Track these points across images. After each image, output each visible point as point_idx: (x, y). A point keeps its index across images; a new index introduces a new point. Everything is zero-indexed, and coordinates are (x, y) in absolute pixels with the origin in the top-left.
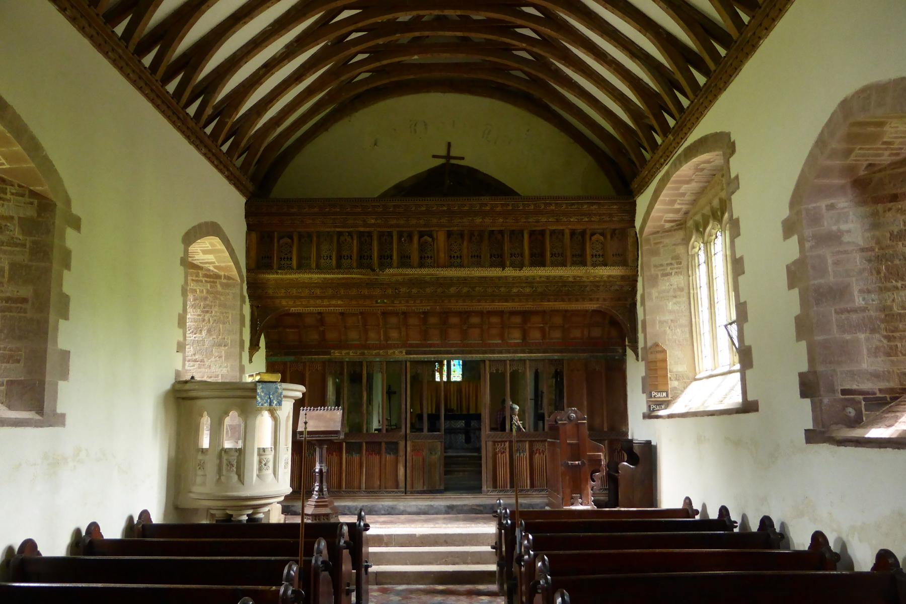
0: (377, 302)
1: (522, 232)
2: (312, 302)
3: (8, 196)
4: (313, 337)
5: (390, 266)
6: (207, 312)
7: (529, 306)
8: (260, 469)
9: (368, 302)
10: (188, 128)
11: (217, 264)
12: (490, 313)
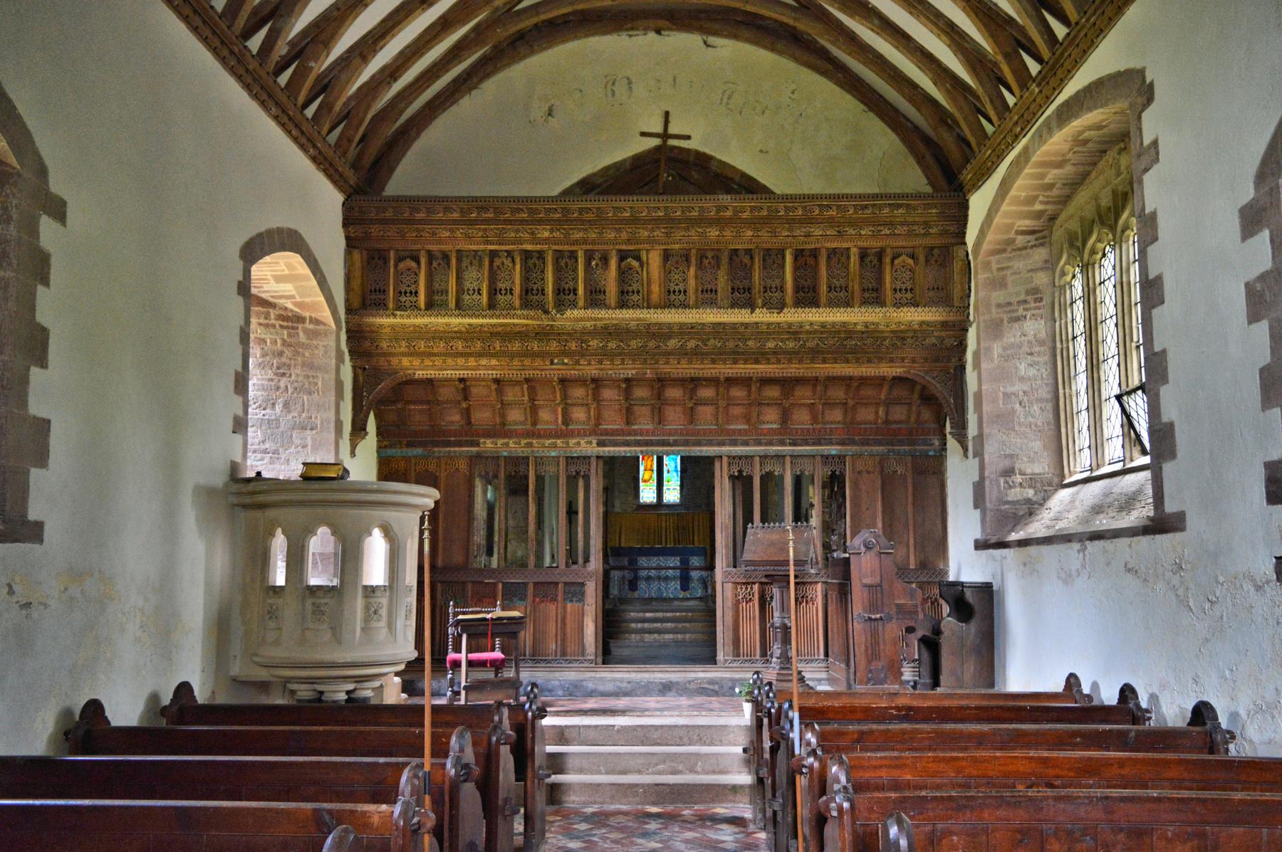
0: (552, 363)
1: (782, 253)
4: (454, 418)
5: (574, 305)
6: (284, 374)
7: (793, 370)
8: (367, 619)
9: (538, 362)
10: (247, 70)
11: (298, 299)
12: (731, 381)
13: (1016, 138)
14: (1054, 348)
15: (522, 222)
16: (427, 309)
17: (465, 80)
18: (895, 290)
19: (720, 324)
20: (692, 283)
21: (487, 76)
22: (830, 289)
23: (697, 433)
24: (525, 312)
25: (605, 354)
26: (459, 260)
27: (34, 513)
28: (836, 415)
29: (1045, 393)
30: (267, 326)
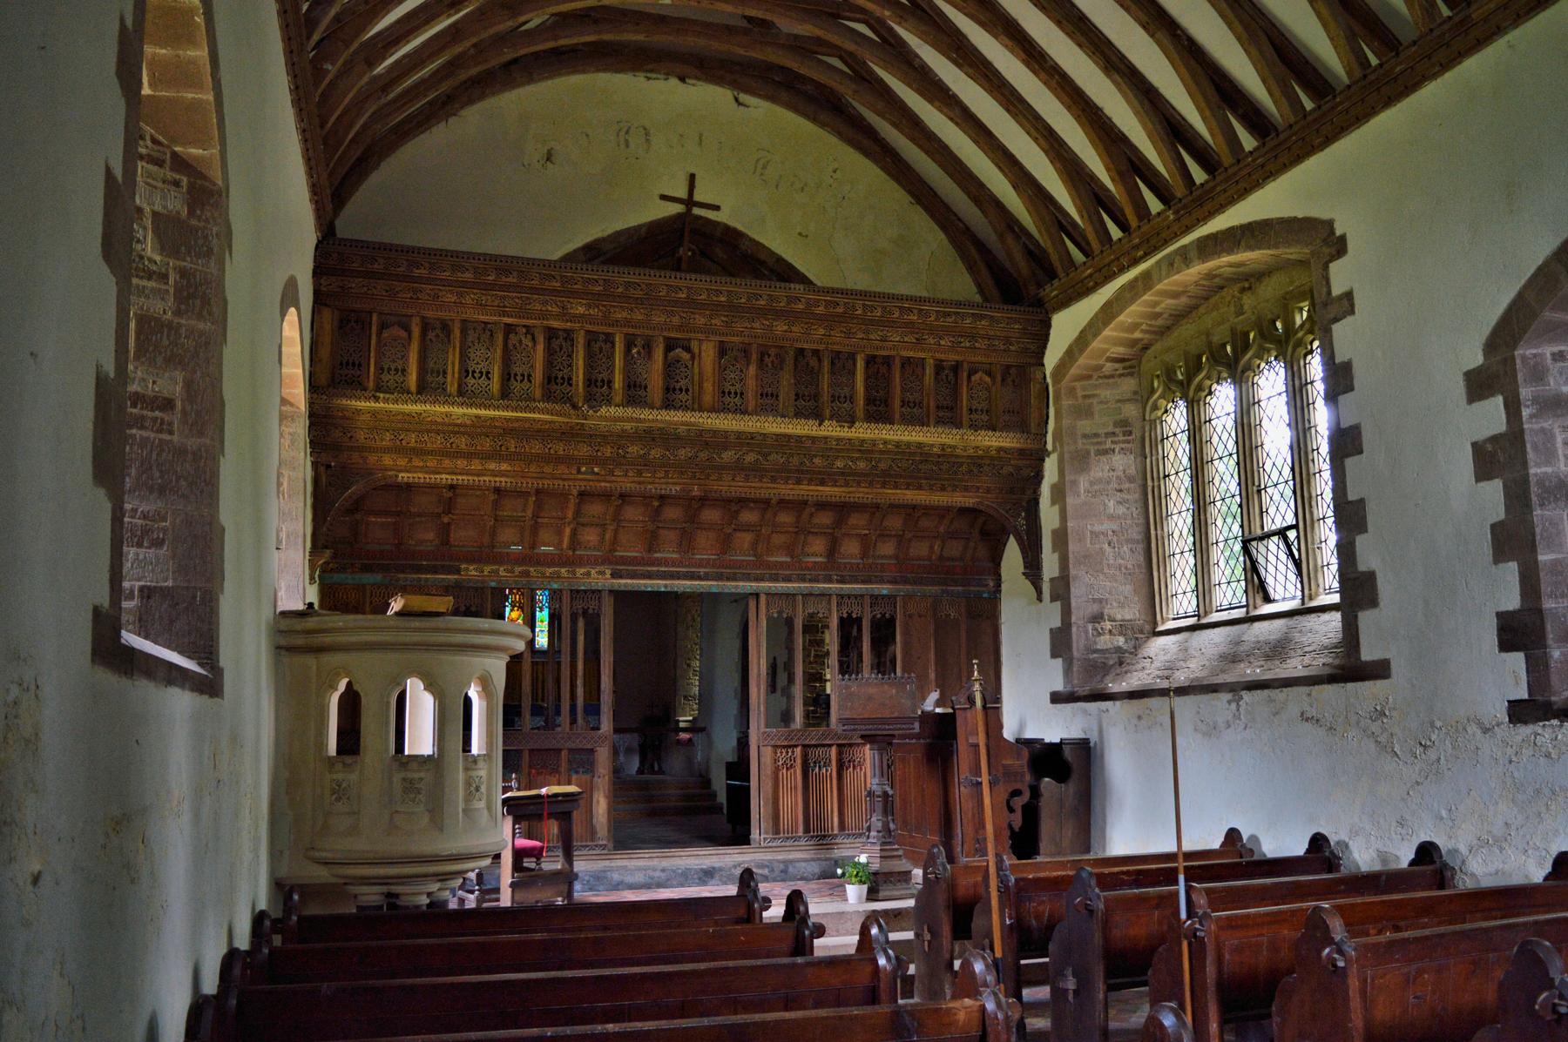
0: (579, 472)
1: (852, 357)
2: (447, 462)
4: (426, 537)
5: (609, 403)
7: (861, 494)
8: (469, 797)
13: (1135, 262)
14: (1145, 486)
15: (555, 292)
16: (419, 392)
20: (751, 383)
22: (904, 403)
25: (645, 463)
26: (464, 331)
29: (1136, 533)
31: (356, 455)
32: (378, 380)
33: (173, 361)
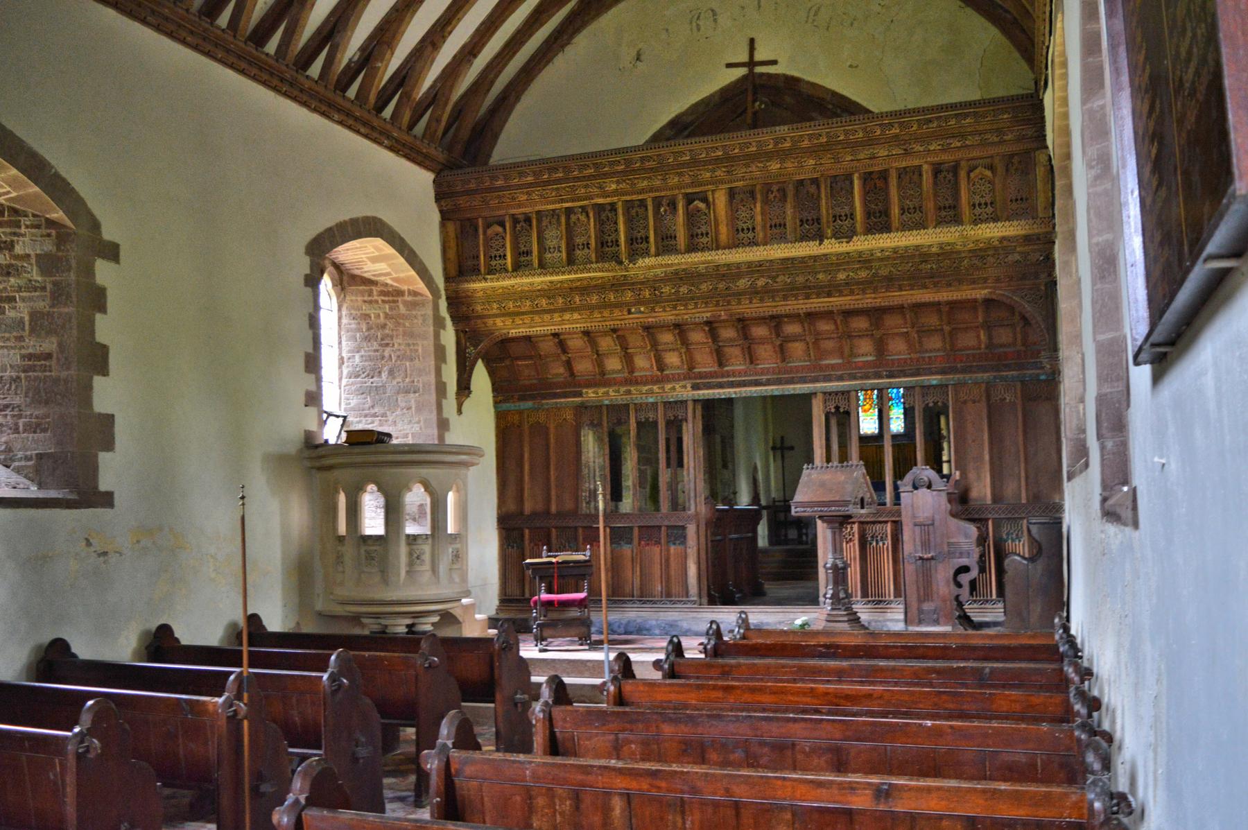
0: (629, 312)
1: (849, 177)
3: (23, 230)
5: (646, 253)
6: (387, 345)
7: (869, 300)
8: (411, 564)
9: (617, 313)
17: (556, 39)
18: (974, 205)
19: (788, 259)
21: (577, 31)
22: (903, 211)
23: (791, 370)
24: (600, 265)
25: (677, 300)
26: (539, 221)
27: (105, 483)
28: (934, 343)
30: (371, 302)
31: (479, 321)
32: (488, 265)
33: (50, 332)
